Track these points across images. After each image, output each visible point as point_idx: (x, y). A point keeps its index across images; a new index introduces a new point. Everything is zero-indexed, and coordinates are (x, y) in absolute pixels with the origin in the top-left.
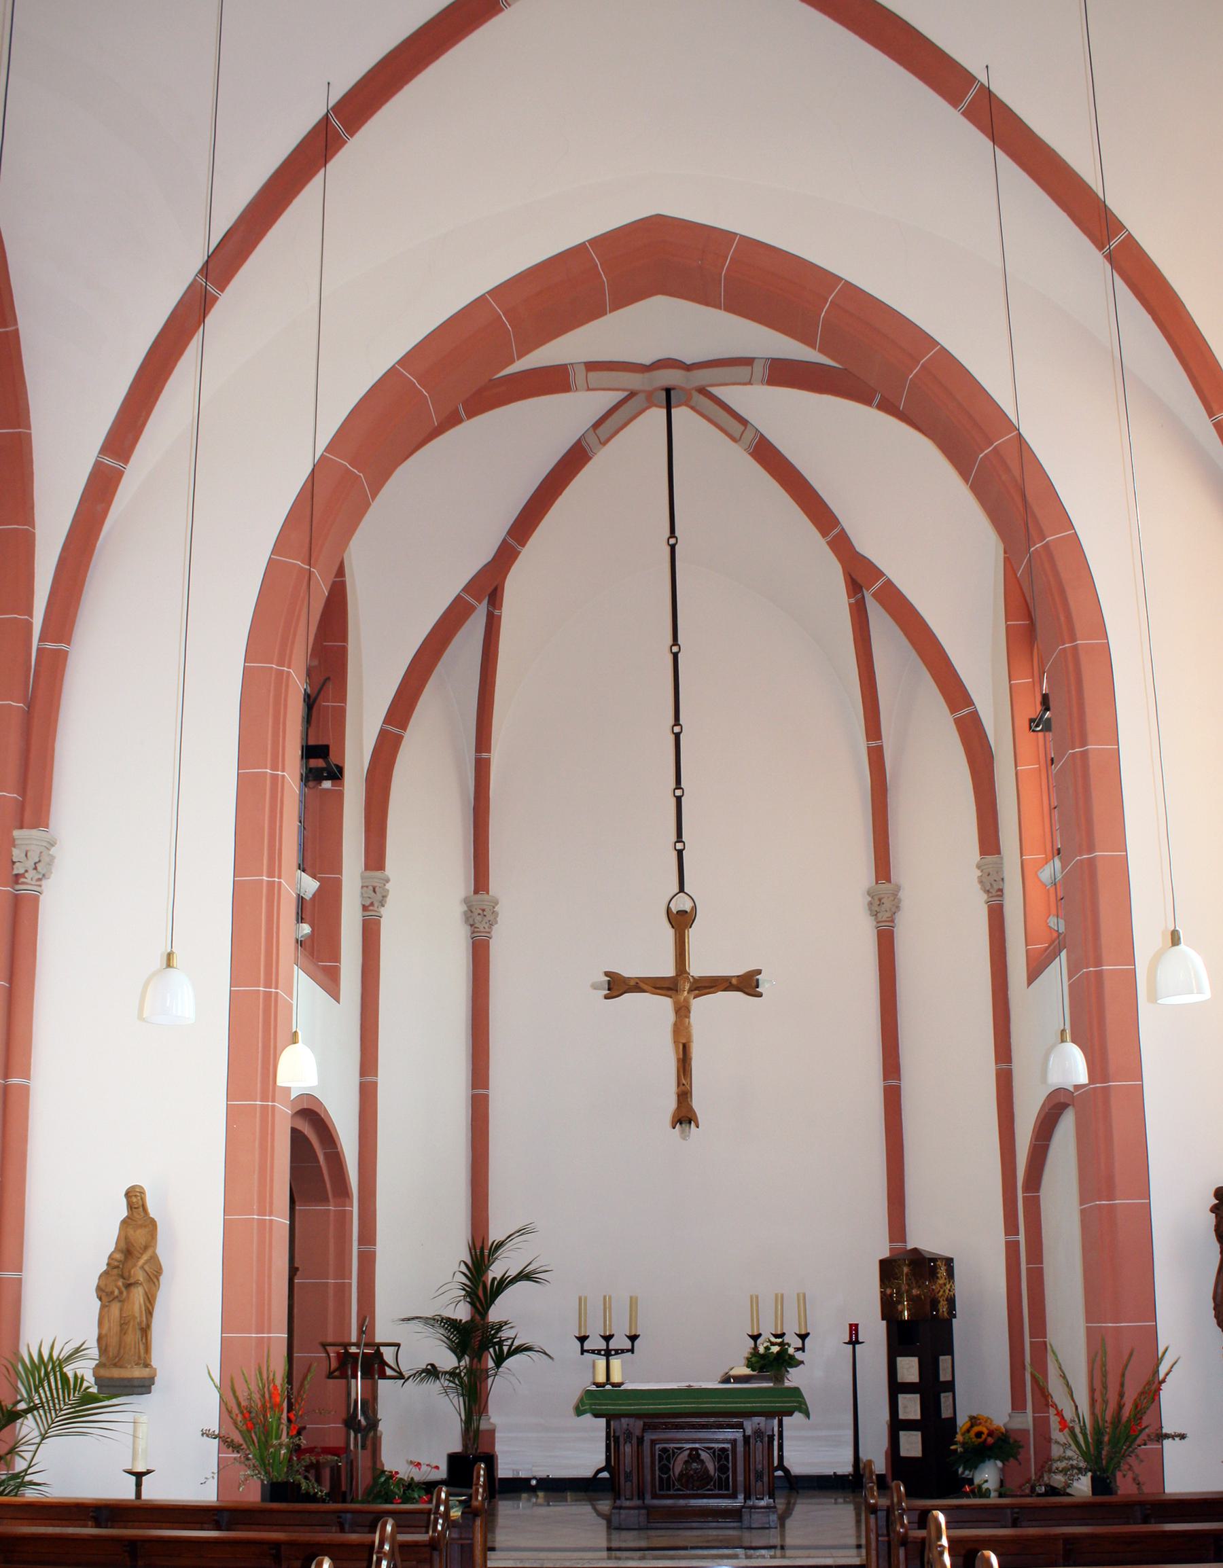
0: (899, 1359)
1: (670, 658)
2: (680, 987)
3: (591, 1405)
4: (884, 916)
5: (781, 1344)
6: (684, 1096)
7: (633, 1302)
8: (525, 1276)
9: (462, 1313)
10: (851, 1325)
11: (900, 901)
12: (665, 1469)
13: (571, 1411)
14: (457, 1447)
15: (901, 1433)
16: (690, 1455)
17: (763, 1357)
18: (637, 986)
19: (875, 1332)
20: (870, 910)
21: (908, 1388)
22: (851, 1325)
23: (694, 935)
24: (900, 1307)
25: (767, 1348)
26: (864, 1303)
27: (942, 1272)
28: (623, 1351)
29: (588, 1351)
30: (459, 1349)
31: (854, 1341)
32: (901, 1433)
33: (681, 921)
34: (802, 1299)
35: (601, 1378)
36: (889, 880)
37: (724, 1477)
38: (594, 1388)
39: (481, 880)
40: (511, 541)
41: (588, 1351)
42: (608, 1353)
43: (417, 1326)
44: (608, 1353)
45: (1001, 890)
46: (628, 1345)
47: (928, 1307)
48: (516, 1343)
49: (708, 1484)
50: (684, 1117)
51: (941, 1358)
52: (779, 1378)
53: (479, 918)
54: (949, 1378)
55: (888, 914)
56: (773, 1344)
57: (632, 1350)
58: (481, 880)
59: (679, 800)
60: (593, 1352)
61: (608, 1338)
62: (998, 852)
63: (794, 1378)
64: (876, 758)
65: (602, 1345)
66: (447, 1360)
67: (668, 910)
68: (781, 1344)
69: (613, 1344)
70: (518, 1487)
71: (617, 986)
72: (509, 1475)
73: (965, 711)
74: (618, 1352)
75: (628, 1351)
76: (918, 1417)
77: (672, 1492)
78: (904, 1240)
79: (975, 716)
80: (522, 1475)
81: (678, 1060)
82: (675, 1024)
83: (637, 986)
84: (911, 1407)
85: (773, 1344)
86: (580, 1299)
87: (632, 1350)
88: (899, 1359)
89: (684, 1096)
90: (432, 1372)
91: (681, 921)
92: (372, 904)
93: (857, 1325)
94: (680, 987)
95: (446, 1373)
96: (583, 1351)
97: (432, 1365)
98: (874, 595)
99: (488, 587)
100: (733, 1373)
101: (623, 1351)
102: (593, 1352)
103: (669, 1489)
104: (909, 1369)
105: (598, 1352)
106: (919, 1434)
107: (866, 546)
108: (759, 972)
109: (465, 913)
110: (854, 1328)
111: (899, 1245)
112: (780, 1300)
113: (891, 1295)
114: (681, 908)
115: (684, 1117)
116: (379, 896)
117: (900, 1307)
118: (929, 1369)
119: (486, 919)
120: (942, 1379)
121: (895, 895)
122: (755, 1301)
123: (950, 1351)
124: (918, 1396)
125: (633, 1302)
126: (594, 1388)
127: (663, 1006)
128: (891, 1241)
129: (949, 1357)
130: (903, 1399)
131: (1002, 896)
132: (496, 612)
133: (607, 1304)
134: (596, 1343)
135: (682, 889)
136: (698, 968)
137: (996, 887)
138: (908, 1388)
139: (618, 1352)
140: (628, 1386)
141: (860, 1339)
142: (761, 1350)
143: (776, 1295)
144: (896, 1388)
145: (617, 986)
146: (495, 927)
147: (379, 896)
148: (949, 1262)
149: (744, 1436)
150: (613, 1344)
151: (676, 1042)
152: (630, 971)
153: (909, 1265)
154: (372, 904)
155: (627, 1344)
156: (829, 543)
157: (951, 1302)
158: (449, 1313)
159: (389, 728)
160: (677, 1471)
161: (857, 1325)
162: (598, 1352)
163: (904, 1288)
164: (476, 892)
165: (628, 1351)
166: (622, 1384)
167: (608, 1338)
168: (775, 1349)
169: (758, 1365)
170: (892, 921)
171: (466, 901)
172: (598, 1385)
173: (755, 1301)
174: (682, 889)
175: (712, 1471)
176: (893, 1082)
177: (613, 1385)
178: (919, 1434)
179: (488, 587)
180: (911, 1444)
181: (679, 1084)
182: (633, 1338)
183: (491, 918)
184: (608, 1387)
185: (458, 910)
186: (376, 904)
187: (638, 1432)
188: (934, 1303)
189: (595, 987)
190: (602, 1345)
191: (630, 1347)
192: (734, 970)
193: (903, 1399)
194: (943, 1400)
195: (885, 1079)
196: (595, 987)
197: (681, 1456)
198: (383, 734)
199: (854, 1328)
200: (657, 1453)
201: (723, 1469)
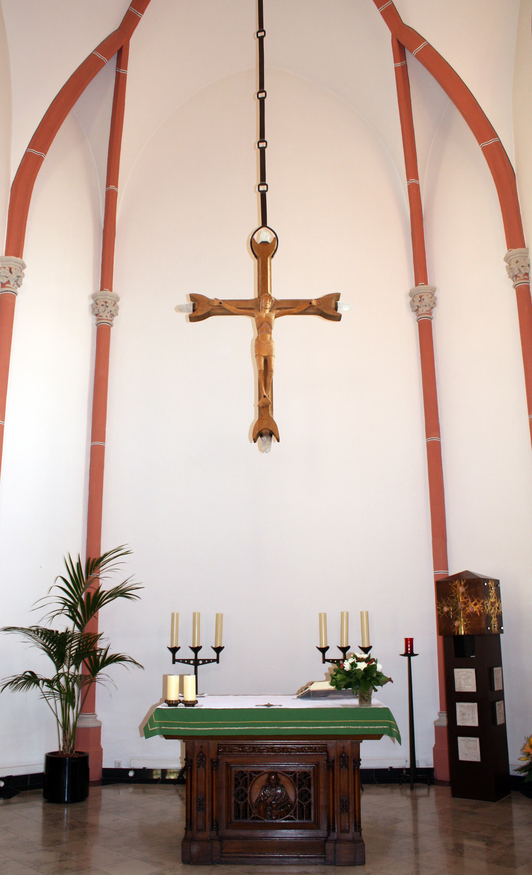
0: (457, 671)
1: (256, 153)
2: (262, 308)
3: (161, 725)
4: (423, 310)
5: (368, 660)
6: (265, 407)
7: (219, 618)
8: (120, 592)
9: (63, 624)
10: (406, 640)
11: (436, 298)
12: (242, 795)
13: (136, 733)
14: (55, 747)
15: (460, 739)
16: (269, 779)
17: (348, 673)
18: (222, 308)
19: (428, 645)
20: (412, 306)
21: (466, 697)
22: (406, 640)
23: (275, 264)
24: (456, 624)
25: (353, 665)
26: (421, 621)
27: (493, 592)
28: (209, 661)
29: (179, 661)
30: (59, 658)
31: (409, 653)
32: (460, 739)
33: (263, 252)
34: (365, 617)
35: (173, 695)
36: (426, 283)
37: (305, 804)
38: (164, 706)
39: (106, 279)
40: (133, 10)
41: (179, 661)
42: (196, 663)
43: (19, 636)
44: (196, 663)
45: (527, 274)
46: (214, 656)
47: (483, 624)
48: (108, 655)
49: (288, 812)
50: (265, 430)
51: (495, 669)
52: (365, 698)
53: (102, 308)
54: (501, 688)
55: (428, 308)
56: (360, 660)
57: (217, 661)
58: (106, 279)
59: (262, 151)
60: (183, 661)
61: (196, 650)
62: (523, 245)
63: (379, 698)
64: (414, 193)
65: (191, 655)
66: (46, 668)
67: (252, 242)
68: (368, 660)
69: (201, 655)
70: (117, 777)
71: (201, 309)
72: (112, 766)
73: (491, 141)
74: (205, 662)
75: (214, 661)
76: (476, 724)
77: (249, 821)
78: (446, 568)
79: (499, 145)
80: (124, 766)
81: (260, 371)
82: (257, 340)
83: (222, 308)
84: (468, 715)
85: (360, 660)
86: (173, 615)
87: (217, 661)
88: (457, 671)
89: (265, 407)
90: (31, 679)
91: (263, 252)
92: (8, 282)
93: (411, 640)
94: (262, 308)
95: (45, 680)
96: (174, 661)
97: (31, 672)
98: (418, 56)
99: (116, 49)
100: (312, 688)
101: (209, 661)
102: (183, 661)
103: (245, 817)
104: (466, 679)
105: (188, 662)
106: (477, 740)
107: (411, 18)
108: (337, 296)
109: (92, 305)
110: (409, 642)
111: (442, 572)
112: (345, 617)
113: (448, 612)
114: (264, 240)
115: (265, 430)
116: (14, 276)
117: (456, 624)
118: (485, 679)
119: (108, 310)
120: (496, 688)
121: (432, 293)
122: (323, 618)
123: (500, 665)
124: (476, 704)
125: (219, 618)
126: (164, 706)
127: (244, 326)
128: (435, 568)
129: (499, 668)
130: (461, 707)
131: (528, 279)
132: (122, 71)
133: (196, 618)
134: (185, 653)
135: (264, 223)
136: (279, 291)
137: (523, 271)
138: (466, 697)
139: (205, 662)
140: (205, 704)
141: (415, 652)
142: (347, 666)
143: (342, 613)
144: (451, 697)
145: (201, 309)
146: (116, 318)
147: (14, 276)
148: (497, 582)
149: (327, 761)
150: (201, 655)
151: (258, 355)
152: (214, 293)
153: (465, 586)
154: (8, 282)
155: (213, 655)
156: (382, 13)
157: (499, 617)
158: (46, 625)
159: (33, 151)
160: (254, 799)
161: (411, 640)
162: (188, 662)
163: (461, 606)
164: (102, 289)
165: (214, 661)
166: (196, 702)
167: (196, 650)
168: (362, 666)
169: (343, 683)
170: (430, 314)
171: (94, 297)
172: (170, 703)
173: (323, 618)
174: (264, 223)
175: (292, 798)
176: (435, 439)
177: (187, 703)
178: (477, 740)
179: (116, 49)
180: (469, 750)
181: (260, 396)
182: (218, 650)
183: (113, 309)
184: (181, 706)
185: (86, 303)
186: (12, 283)
187: (212, 755)
188: (488, 618)
189: (180, 309)
190: (191, 655)
191: (215, 658)
192: (314, 293)
193: (461, 707)
194: (497, 708)
195: (428, 436)
196: (180, 309)
197: (259, 781)
198: (27, 156)
199: (409, 642)
200: (233, 774)
201: (304, 795)
